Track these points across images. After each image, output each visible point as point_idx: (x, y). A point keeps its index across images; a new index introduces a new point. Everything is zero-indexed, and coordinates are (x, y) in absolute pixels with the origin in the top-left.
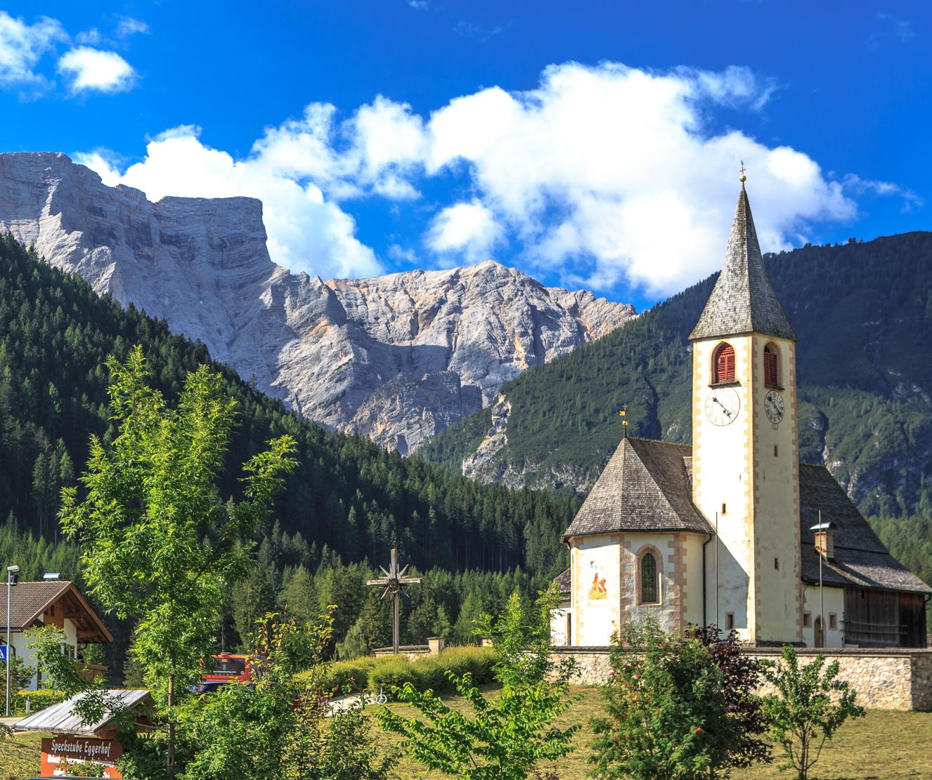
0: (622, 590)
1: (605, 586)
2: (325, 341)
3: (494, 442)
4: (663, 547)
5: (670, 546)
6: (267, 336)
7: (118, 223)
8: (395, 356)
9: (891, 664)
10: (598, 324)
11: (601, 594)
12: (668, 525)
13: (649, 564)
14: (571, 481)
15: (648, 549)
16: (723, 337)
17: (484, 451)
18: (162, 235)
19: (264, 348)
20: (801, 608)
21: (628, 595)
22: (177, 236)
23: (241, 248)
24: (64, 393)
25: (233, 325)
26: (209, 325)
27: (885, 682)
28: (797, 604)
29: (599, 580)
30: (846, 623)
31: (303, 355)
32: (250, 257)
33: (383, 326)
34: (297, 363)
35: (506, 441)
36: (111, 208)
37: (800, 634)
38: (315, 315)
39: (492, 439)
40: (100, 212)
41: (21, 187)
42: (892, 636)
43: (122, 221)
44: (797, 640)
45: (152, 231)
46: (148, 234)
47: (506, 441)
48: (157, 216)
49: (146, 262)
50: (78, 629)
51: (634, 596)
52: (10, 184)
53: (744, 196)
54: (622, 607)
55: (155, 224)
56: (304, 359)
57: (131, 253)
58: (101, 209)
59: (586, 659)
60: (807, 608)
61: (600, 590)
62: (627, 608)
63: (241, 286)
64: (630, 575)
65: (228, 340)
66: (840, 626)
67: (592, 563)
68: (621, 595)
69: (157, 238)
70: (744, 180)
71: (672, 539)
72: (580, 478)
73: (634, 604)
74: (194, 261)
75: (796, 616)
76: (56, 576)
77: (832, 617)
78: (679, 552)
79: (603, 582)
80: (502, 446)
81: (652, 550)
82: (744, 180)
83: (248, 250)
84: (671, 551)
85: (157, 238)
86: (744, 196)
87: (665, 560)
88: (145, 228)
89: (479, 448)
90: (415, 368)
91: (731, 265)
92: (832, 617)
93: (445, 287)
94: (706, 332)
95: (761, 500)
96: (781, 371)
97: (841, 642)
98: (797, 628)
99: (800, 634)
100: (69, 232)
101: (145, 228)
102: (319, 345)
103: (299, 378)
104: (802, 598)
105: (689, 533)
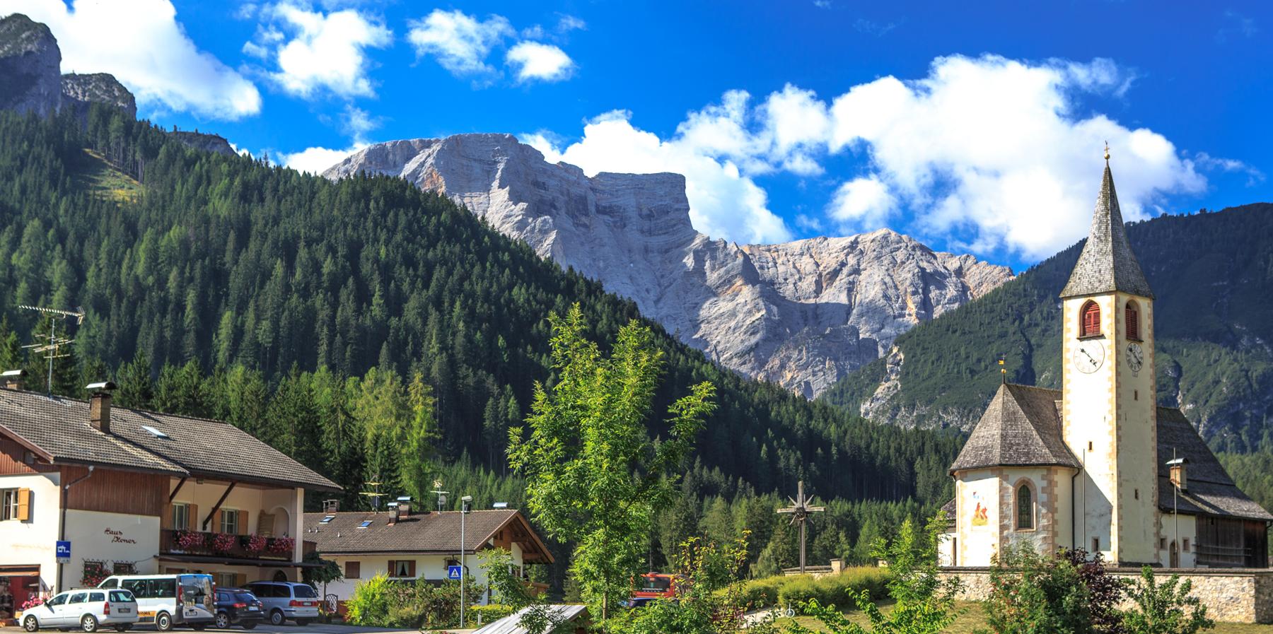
0: (1001, 517)
1: (987, 513)
3: (889, 388)
5: (1043, 479)
9: (1237, 582)
10: (980, 284)
12: (1041, 461)
14: (956, 422)
15: (1024, 481)
16: (1089, 295)
17: (879, 396)
18: (597, 206)
20: (1158, 533)
21: (1006, 522)
22: (610, 207)
24: (512, 344)
26: (638, 285)
27: (1232, 598)
29: (981, 508)
31: (721, 311)
32: (675, 225)
33: (791, 286)
34: (716, 318)
35: (899, 386)
36: (552, 183)
37: (1157, 556)
39: (887, 385)
40: (543, 186)
42: (1238, 558)
43: (562, 194)
44: (1155, 561)
45: (589, 202)
47: (899, 386)
48: (593, 190)
49: (583, 229)
50: (524, 552)
51: (1011, 522)
52: (464, 162)
53: (1108, 172)
54: (1001, 532)
55: (591, 197)
56: (722, 315)
57: (570, 222)
58: (544, 183)
59: (969, 578)
60: (1163, 533)
61: (982, 518)
62: (1005, 533)
63: (667, 251)
64: (1008, 504)
68: (1000, 522)
70: (1108, 158)
72: (964, 419)
73: (1012, 530)
74: (626, 229)
75: (1154, 540)
78: (1051, 484)
79: (985, 510)
80: (895, 391)
81: (1027, 482)
82: (1108, 158)
84: (1045, 483)
85: (592, 209)
86: (1108, 172)
87: (1039, 490)
88: (583, 200)
91: (1096, 232)
94: (1075, 291)
95: (1122, 439)
98: (1155, 551)
99: (1157, 556)
101: (583, 200)
102: (735, 303)
104: (1159, 525)
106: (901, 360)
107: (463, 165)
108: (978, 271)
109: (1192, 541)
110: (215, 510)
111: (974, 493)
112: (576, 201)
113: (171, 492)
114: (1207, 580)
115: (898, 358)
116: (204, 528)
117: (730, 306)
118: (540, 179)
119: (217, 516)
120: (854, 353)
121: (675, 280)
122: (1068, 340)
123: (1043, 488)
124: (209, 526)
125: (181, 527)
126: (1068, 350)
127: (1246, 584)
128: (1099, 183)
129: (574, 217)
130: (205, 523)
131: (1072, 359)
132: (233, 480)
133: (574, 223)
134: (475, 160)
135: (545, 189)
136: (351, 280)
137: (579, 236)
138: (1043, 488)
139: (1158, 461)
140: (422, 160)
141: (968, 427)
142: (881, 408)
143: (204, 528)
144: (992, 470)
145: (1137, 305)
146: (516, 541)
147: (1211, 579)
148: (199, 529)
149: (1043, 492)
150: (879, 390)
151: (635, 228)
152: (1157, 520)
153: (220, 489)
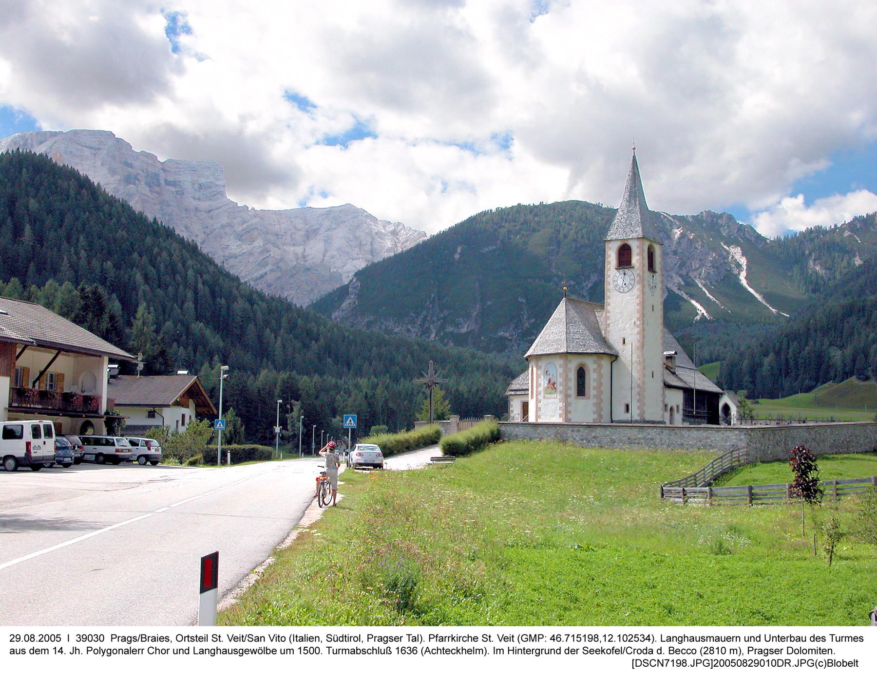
2: (256, 244)
3: (350, 303)
4: (591, 365)
5: (594, 363)
6: (224, 240)
7: (141, 172)
8: (295, 254)
9: (736, 435)
10: (407, 241)
11: (552, 391)
13: (581, 374)
14: (392, 326)
15: (581, 364)
17: (344, 308)
18: (166, 180)
19: (222, 246)
20: (663, 401)
22: (175, 182)
23: (210, 190)
24: (117, 267)
25: (204, 233)
26: (191, 232)
27: (733, 445)
28: (661, 399)
29: (552, 382)
30: (684, 410)
31: (244, 251)
32: (215, 195)
33: (289, 237)
34: (240, 255)
35: (357, 303)
36: (136, 164)
37: (663, 416)
38: (251, 229)
39: (349, 302)
40: (131, 166)
41: (85, 149)
42: (704, 417)
43: (143, 171)
44: (662, 420)
45: (161, 178)
46: (158, 180)
47: (357, 303)
48: (164, 170)
49: (156, 195)
50: (196, 406)
52: (79, 147)
53: (634, 157)
55: (162, 175)
56: (244, 254)
57: (147, 189)
58: (131, 164)
59: (550, 430)
60: (666, 401)
63: (210, 211)
65: (201, 241)
66: (681, 412)
67: (547, 372)
69: (163, 182)
70: (634, 149)
71: (596, 359)
72: (396, 325)
74: (184, 196)
75: (661, 406)
76: (186, 372)
77: (678, 406)
78: (600, 366)
79: (554, 384)
80: (354, 306)
81: (583, 365)
82: (634, 149)
83: (213, 191)
84: (595, 366)
85: (163, 182)
86: (634, 157)
88: (156, 176)
89: (342, 306)
90: (306, 261)
92: (678, 406)
93: (323, 217)
94: (614, 237)
95: (646, 337)
96: (655, 262)
97: (681, 421)
98: (662, 412)
99: (663, 416)
100: (113, 176)
101: (156, 176)
102: (252, 246)
103: (241, 264)
104: (664, 395)
105: (605, 355)
106: (358, 286)
107: (78, 149)
108: (405, 233)
109: (681, 407)
110: (42, 373)
111: (547, 372)
112: (151, 177)
113: (17, 354)
114: (717, 433)
115: (356, 285)
116: (34, 386)
117: (249, 247)
118: (129, 161)
119: (44, 377)
120: (327, 281)
121: (214, 230)
122: (609, 269)
123: (594, 369)
124: (37, 384)
125: (17, 385)
126: (609, 276)
127: (742, 437)
128: (631, 162)
129: (150, 186)
130: (34, 383)
131: (611, 282)
132: (60, 349)
133: (150, 190)
134: (86, 147)
135: (132, 168)
136: (9, 220)
137: (153, 199)
138: (594, 369)
139: (685, 351)
140: (50, 145)
141: (399, 329)
142: (345, 316)
143: (34, 386)
144: (560, 356)
145: (653, 247)
146: (192, 398)
147: (720, 434)
148: (30, 387)
149: (594, 372)
150: (344, 305)
151: (189, 195)
152: (663, 392)
153: (48, 356)
